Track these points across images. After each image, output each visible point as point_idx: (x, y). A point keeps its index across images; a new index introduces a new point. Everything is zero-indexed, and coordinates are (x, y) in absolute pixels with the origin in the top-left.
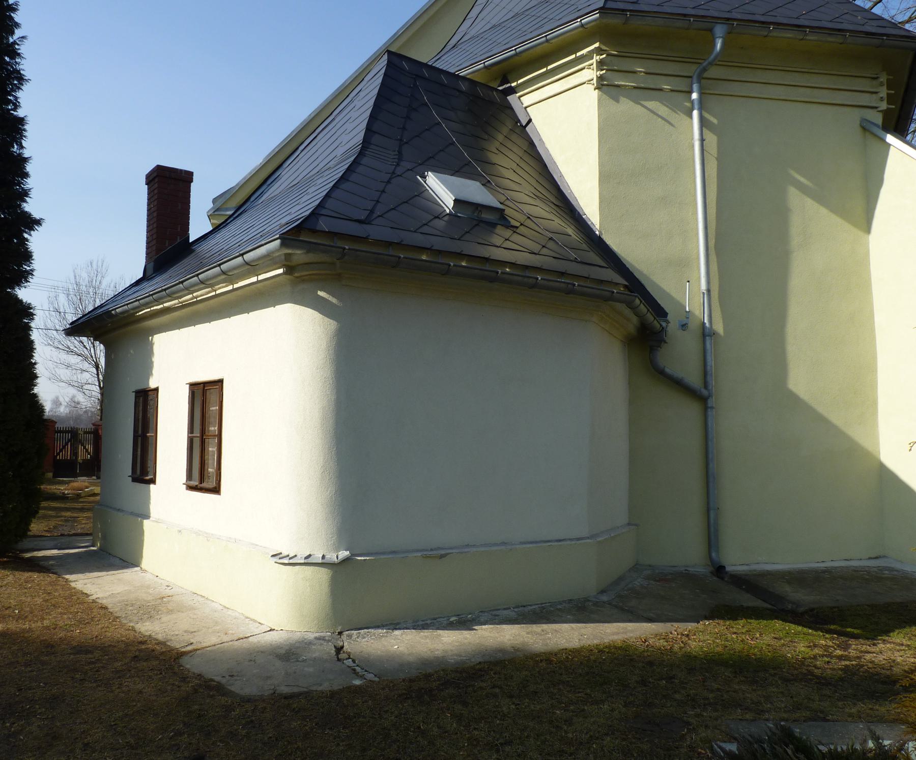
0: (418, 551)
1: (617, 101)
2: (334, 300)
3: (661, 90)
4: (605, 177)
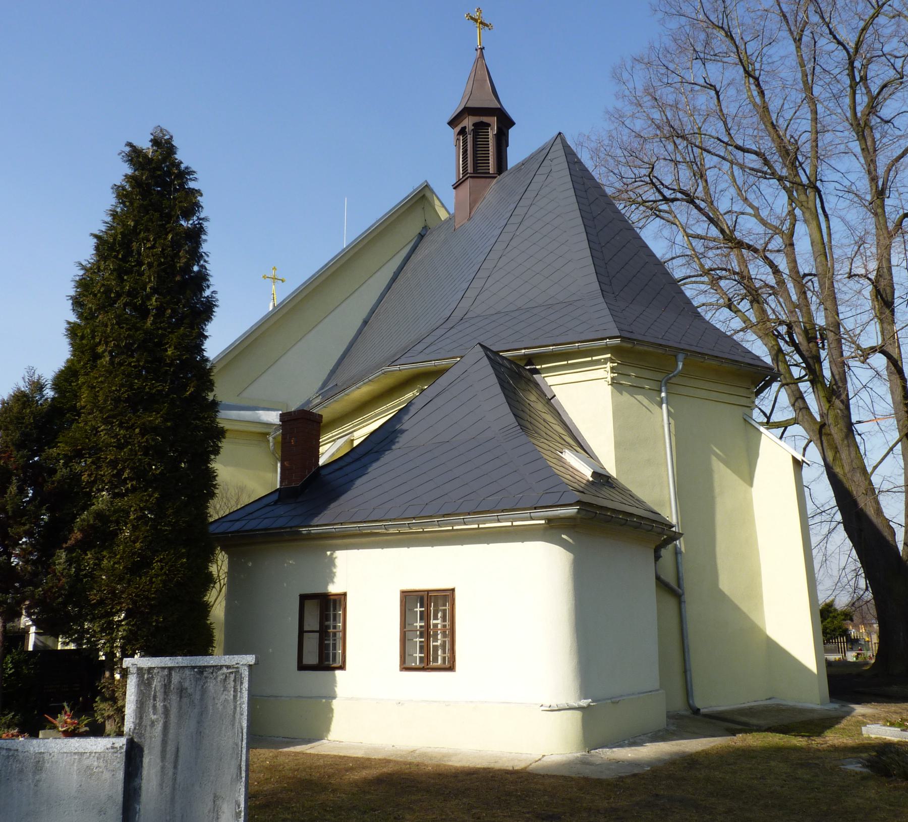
0: (608, 699)
1: (622, 394)
2: (571, 541)
3: (644, 388)
4: (618, 445)
